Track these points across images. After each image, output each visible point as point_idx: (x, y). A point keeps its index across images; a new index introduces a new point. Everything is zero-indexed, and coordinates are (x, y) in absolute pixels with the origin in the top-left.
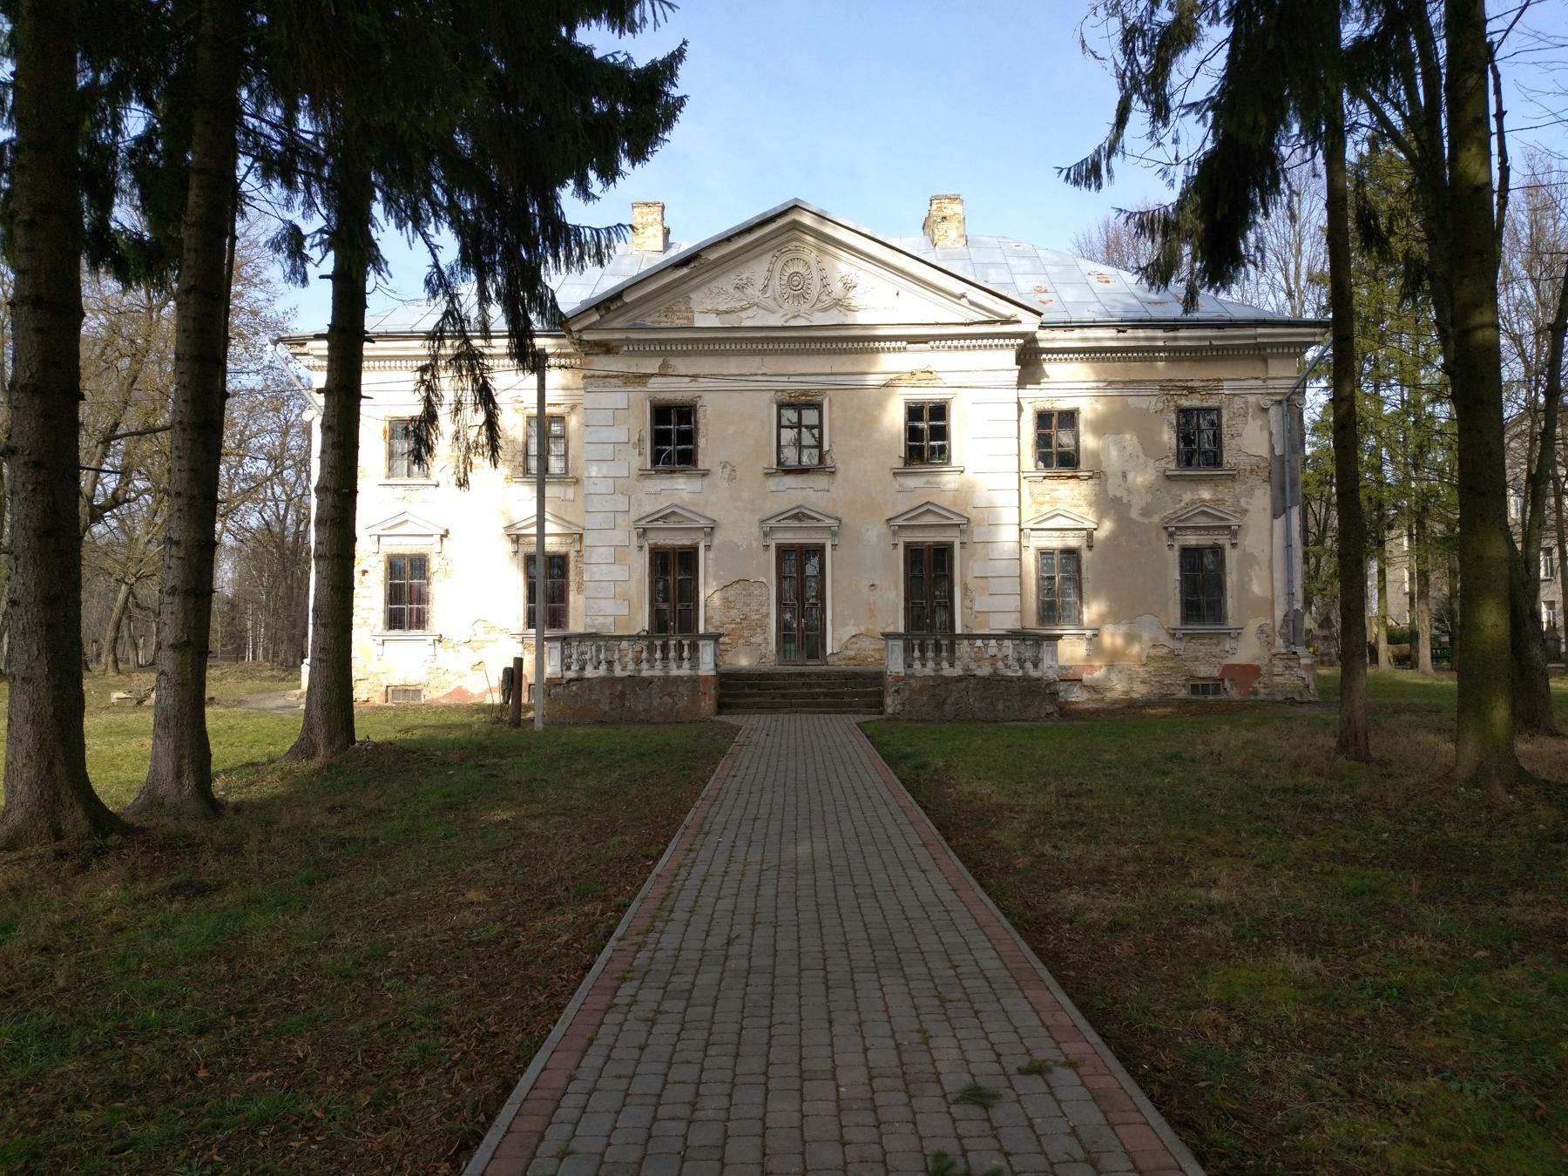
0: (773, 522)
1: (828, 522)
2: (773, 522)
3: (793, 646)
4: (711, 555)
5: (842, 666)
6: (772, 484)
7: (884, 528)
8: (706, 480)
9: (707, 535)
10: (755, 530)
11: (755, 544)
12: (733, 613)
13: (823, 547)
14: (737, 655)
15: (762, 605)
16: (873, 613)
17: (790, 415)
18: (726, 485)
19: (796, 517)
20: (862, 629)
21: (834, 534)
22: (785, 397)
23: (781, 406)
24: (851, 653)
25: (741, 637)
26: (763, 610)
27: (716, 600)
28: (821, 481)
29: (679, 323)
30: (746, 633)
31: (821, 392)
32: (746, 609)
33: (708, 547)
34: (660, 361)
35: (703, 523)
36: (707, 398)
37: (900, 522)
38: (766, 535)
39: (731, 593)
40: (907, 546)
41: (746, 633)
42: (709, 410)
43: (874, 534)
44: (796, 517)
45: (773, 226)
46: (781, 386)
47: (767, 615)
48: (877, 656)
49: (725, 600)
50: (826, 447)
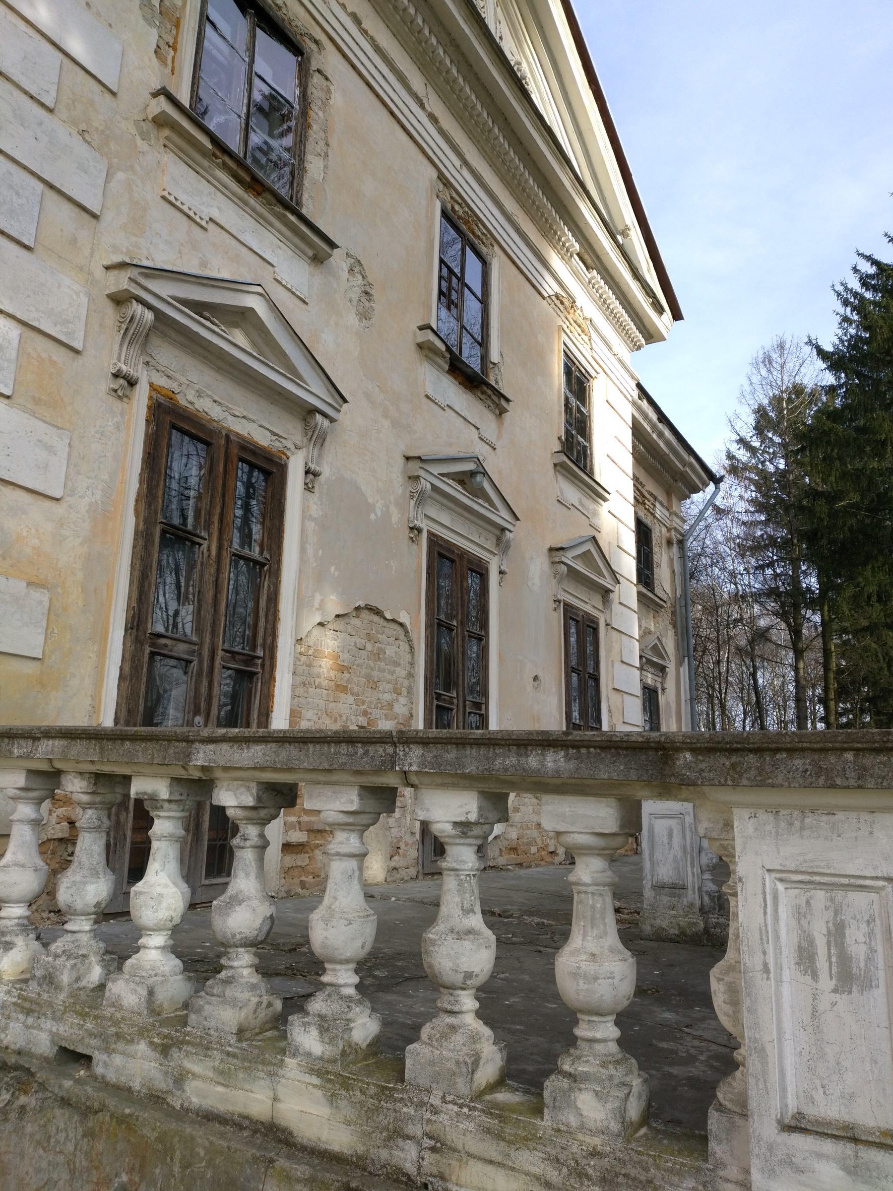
19: (464, 479)
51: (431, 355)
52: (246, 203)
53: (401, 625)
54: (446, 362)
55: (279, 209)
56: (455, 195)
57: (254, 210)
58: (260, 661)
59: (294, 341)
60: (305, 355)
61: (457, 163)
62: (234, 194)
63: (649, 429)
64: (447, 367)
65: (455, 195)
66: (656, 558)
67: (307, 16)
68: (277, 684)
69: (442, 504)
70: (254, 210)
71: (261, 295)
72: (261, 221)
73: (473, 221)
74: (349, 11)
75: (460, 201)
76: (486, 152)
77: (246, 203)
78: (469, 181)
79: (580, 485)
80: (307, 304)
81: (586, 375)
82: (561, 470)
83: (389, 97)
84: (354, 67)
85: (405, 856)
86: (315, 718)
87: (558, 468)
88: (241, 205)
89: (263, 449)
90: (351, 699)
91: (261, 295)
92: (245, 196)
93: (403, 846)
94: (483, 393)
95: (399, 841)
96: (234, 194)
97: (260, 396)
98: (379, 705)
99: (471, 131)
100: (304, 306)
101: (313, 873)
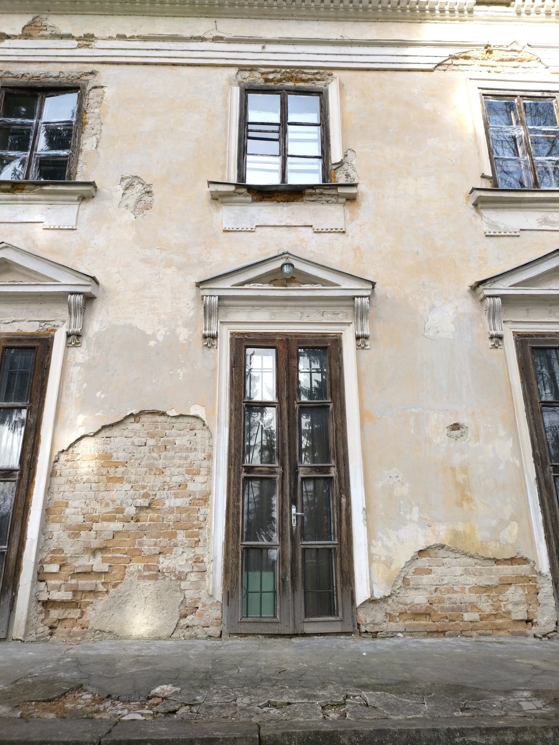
0: (226, 287)
1: (348, 287)
2: (226, 287)
3: (268, 580)
4: (79, 355)
5: (401, 646)
6: (228, 216)
7: (468, 305)
8: (88, 208)
9: (72, 311)
10: (188, 305)
11: (183, 334)
12: (120, 493)
13: (337, 341)
14: (120, 604)
15: (193, 472)
16: (464, 495)
17: (264, 110)
18: (128, 216)
19: (279, 278)
20: (442, 534)
21: (361, 314)
22: (257, 79)
23: (248, 90)
24: (419, 599)
25: (134, 554)
26: (196, 486)
27: (86, 459)
28: (330, 214)
29: (73, 388)
30: (148, 545)
31: (325, 72)
32: (153, 482)
33: (74, 338)
34: (27, 19)
35: (66, 282)
36: (106, 74)
37: (503, 287)
38: (209, 312)
39: (120, 441)
40: (522, 340)
41: (148, 545)
42: (108, 92)
43: (448, 318)
44: (279, 278)
45: (243, 416)
46: (250, 54)
47: (205, 499)
48: (487, 607)
49: (106, 459)
50: (336, 156)
51: (225, 199)
52: (17, 200)
53: (196, 417)
54: (246, 196)
55: (38, 189)
56: (264, 70)
57: (23, 200)
58: (18, 473)
59: (40, 260)
60: (55, 267)
61: (258, 47)
62: (6, 200)
63: (67, 174)
64: (250, 199)
65: (264, 70)
66: (15, 556)
67: (80, 65)
68: (35, 486)
69: (253, 306)
70: (23, 200)
71: (7, 247)
72: (32, 202)
73: (297, 73)
74: (115, 36)
75: (272, 70)
76: (305, 16)
77: (17, 200)
78: (96, 58)
79: (536, 205)
80: (75, 229)
81: (546, 94)
82: (484, 205)
83: (166, 57)
84: (128, 64)
85: (201, 615)
86: (83, 505)
87: (480, 206)
88: (15, 202)
89: (32, 334)
90: (127, 486)
91: (7, 247)
92: (14, 196)
93: (200, 605)
94: (311, 195)
95: (196, 602)
96: (6, 200)
97: (30, 303)
98: (166, 487)
99: (279, 15)
100: (75, 231)
101: (81, 625)
